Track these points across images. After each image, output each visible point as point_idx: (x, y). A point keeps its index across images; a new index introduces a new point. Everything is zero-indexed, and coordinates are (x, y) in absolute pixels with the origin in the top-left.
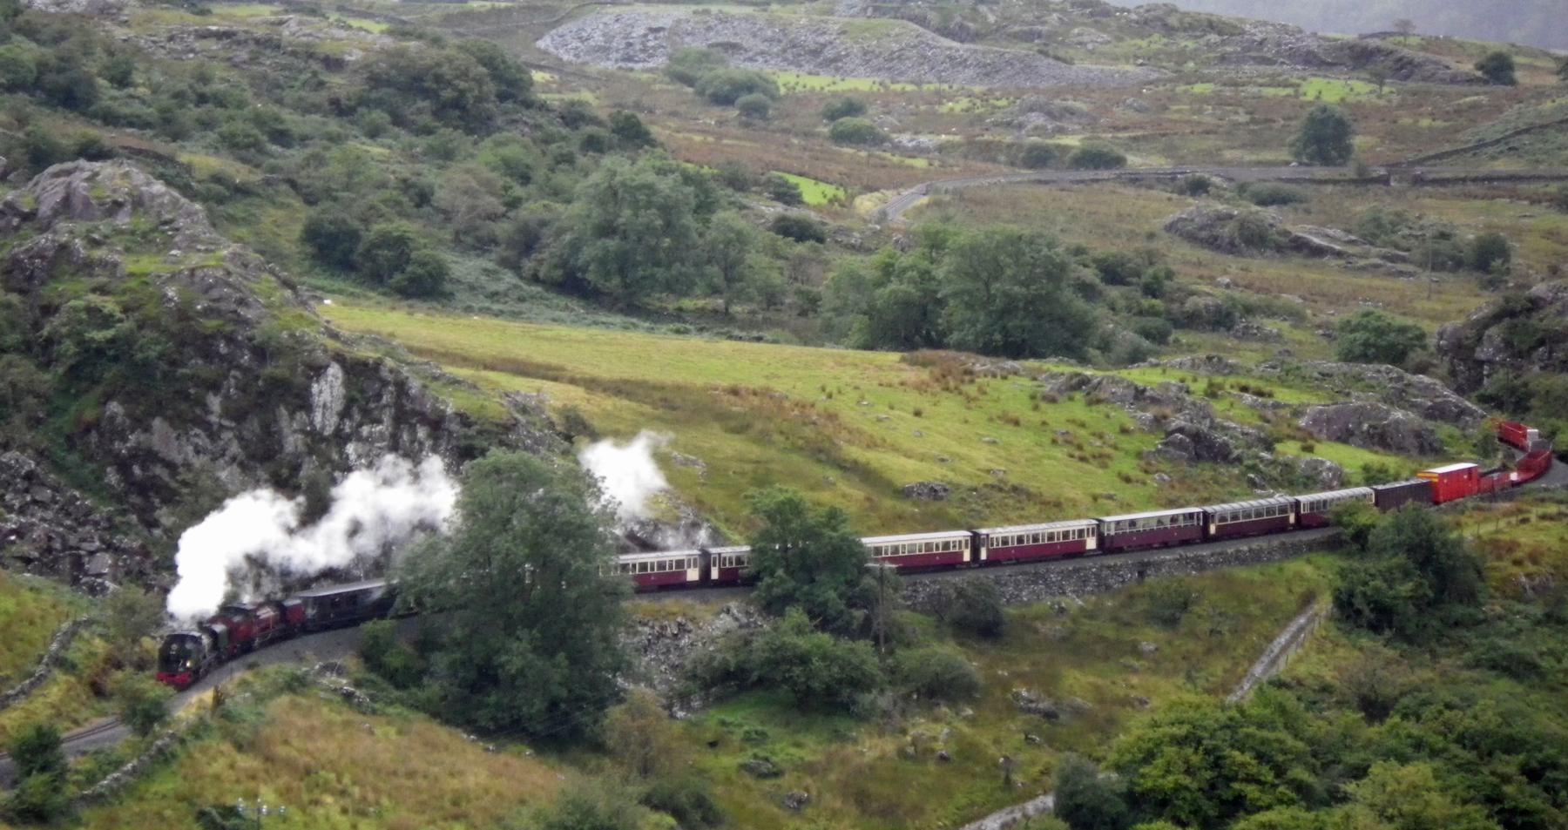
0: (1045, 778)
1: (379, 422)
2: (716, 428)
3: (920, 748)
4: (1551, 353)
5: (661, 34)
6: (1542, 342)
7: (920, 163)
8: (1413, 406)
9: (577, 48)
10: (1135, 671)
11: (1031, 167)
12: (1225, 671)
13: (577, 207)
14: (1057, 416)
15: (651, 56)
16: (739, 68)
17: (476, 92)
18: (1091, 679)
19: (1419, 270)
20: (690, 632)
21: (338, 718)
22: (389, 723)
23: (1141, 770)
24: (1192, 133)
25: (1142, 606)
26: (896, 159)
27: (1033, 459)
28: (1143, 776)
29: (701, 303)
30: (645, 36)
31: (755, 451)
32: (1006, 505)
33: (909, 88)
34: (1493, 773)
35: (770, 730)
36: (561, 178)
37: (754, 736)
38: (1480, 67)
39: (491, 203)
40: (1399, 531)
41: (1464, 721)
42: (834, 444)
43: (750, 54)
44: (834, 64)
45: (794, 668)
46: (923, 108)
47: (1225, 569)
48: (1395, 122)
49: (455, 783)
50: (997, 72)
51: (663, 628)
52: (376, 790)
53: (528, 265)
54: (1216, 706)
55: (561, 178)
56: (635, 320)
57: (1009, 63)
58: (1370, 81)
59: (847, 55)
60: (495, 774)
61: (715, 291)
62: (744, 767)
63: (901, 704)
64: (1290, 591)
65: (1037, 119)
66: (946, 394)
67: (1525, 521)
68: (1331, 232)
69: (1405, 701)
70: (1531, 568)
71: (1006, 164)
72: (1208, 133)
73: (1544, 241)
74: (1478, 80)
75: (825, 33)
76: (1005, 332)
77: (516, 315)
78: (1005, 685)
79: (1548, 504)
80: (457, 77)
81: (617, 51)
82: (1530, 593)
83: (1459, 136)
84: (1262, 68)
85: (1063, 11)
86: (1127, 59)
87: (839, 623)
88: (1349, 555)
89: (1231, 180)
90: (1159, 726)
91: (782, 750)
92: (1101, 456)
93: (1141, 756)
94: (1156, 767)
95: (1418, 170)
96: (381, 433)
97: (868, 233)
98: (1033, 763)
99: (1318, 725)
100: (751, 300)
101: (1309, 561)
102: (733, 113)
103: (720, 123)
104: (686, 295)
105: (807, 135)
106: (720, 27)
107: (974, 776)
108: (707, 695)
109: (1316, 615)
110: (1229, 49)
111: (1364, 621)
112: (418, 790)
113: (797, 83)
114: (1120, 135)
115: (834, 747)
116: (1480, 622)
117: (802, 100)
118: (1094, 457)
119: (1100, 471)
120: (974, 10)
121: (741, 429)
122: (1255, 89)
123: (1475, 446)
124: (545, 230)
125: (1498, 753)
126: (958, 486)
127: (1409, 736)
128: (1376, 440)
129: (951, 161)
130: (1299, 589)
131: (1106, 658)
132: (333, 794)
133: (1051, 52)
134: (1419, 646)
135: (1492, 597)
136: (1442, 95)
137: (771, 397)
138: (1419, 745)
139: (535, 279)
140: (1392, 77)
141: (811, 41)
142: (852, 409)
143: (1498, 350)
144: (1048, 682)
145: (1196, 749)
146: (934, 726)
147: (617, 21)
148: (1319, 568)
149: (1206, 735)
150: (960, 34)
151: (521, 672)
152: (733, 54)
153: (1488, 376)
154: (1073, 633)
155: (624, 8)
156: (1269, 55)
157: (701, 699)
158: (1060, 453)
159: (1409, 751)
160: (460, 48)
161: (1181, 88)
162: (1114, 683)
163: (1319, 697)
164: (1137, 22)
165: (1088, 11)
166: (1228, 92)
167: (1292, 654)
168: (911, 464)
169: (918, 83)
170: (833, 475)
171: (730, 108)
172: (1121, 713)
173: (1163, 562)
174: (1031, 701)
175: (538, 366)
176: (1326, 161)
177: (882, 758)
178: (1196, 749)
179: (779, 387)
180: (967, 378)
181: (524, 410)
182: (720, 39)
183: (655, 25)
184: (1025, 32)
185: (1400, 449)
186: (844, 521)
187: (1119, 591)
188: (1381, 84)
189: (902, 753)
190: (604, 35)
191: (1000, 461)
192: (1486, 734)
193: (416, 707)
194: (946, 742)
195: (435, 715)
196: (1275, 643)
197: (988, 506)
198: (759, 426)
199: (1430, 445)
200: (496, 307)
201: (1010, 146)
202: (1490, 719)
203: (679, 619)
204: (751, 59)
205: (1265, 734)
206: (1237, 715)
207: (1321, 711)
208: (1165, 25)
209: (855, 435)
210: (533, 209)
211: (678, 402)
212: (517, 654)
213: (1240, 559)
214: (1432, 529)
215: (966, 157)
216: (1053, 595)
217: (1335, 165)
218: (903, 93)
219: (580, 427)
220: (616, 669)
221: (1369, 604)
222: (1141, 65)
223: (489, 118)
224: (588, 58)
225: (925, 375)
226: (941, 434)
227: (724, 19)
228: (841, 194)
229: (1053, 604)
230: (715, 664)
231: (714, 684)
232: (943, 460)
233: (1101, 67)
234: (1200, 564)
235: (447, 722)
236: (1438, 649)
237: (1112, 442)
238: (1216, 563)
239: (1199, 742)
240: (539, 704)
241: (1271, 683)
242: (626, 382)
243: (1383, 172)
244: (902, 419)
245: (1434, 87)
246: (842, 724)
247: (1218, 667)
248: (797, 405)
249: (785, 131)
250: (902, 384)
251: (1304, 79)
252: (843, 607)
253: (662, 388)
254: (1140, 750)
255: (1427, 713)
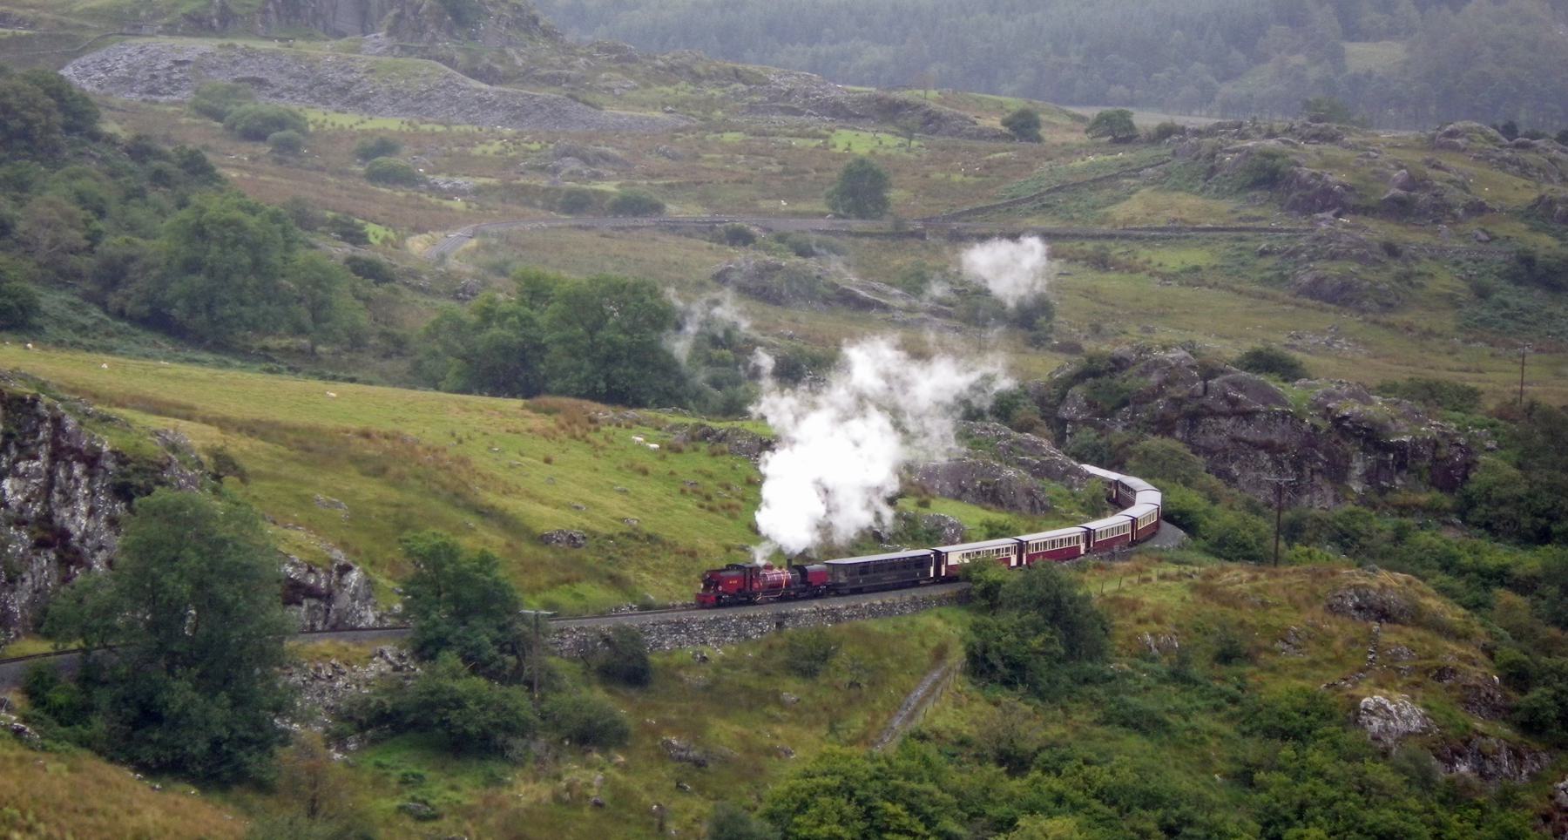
0: (697, 826)
1: (36, 458)
2: (353, 471)
3: (576, 793)
4: (1134, 412)
5: (186, 67)
6: (1125, 403)
7: (458, 204)
8: (1022, 464)
9: (100, 78)
10: (778, 721)
11: (569, 212)
12: (866, 723)
13: (162, 243)
14: (678, 463)
15: (176, 89)
16: (265, 104)
17: (44, 122)
18: (737, 728)
19: (964, 326)
20: (344, 674)
21: (12, 754)
22: (58, 760)
23: (796, 819)
24: (726, 182)
25: (781, 657)
26: (434, 200)
27: (664, 509)
28: (798, 825)
29: (285, 343)
30: (170, 68)
31: (394, 495)
32: (642, 553)
33: (439, 129)
34: (1133, 829)
35: (430, 775)
36: (138, 213)
37: (411, 779)
38: (1005, 123)
39: (76, 236)
40: (1031, 586)
41: (1101, 776)
42: (469, 489)
43: (277, 90)
44: (362, 102)
45: (451, 712)
46: (456, 149)
47: (860, 622)
48: (927, 176)
49: (134, 822)
50: (527, 115)
51: (318, 669)
52: (59, 826)
53: (114, 300)
54: (865, 758)
55: (138, 213)
56: (225, 358)
57: (538, 107)
58: (897, 135)
59: (375, 94)
60: (168, 813)
61: (300, 330)
62: (401, 809)
63: (553, 750)
64: (923, 644)
65: (573, 164)
66: (574, 442)
67: (1146, 580)
68: (875, 285)
69: (1045, 755)
70: (1155, 627)
71: (543, 208)
72: (743, 182)
73: (1083, 299)
74: (1003, 137)
75: (352, 71)
76: (608, 379)
77: (109, 350)
78: (655, 733)
79: (1165, 563)
80: (24, 108)
81: (142, 83)
82: (1155, 651)
83: (992, 191)
84: (789, 118)
85: (590, 56)
86: (654, 105)
87: (492, 667)
88: (981, 610)
89: (769, 230)
90: (813, 777)
91: (439, 793)
92: (730, 506)
93: (795, 806)
94: (810, 818)
95: (955, 225)
96: (37, 468)
97: (437, 276)
98: (686, 811)
99: (957, 777)
100: (337, 341)
101: (940, 616)
102: (264, 149)
103: (254, 159)
104: (267, 333)
105: (342, 173)
106: (246, 62)
107: (628, 821)
108: (363, 738)
109: (950, 669)
110: (756, 98)
111: (998, 677)
112: (99, 828)
113: (325, 121)
114: (656, 182)
115: (490, 791)
116: (1110, 679)
117: (336, 137)
118: (723, 508)
119: (730, 522)
120: (502, 52)
121: (380, 471)
122: (785, 140)
123: (1083, 504)
124: (131, 265)
125: (1136, 809)
126: (594, 534)
127: (1050, 790)
128: (989, 496)
129: (490, 204)
130: (932, 643)
131: (750, 708)
132: (20, 830)
133: (581, 98)
134: (1051, 702)
135: (1119, 655)
136: (972, 150)
137: (403, 441)
138: (1059, 799)
139: (121, 314)
140: (919, 131)
141: (338, 77)
142: (484, 455)
143: (1081, 410)
144: (696, 731)
145: (849, 800)
146: (587, 772)
147: (141, 52)
148: (949, 623)
149: (859, 786)
150: (489, 76)
151: (184, 711)
152: (259, 89)
153: (1071, 435)
154: (716, 682)
155: (147, 40)
156: (796, 106)
157: (357, 741)
158: (690, 504)
159: (1051, 805)
160: (26, 78)
161: (710, 137)
162: (758, 732)
163: (958, 749)
164: (663, 69)
165: (614, 56)
166: (758, 143)
167: (930, 707)
168: (546, 511)
169: (448, 125)
170: (472, 521)
171: (261, 144)
172: (770, 763)
173: (801, 613)
174: (682, 750)
175: (168, 404)
176: (862, 215)
177: (538, 802)
178: (849, 800)
179: (410, 431)
180: (592, 426)
181: (174, 448)
182: (246, 74)
183: (181, 58)
184: (553, 76)
185: (1013, 506)
186: (496, 565)
187: (758, 642)
188: (911, 138)
189: (557, 798)
190: (128, 66)
191: (634, 510)
192: (1124, 790)
193: (84, 743)
194: (600, 789)
195: (100, 753)
196: (912, 696)
197: (625, 555)
198: (394, 469)
199: (1041, 503)
200: (86, 341)
201: (546, 190)
202: (1128, 777)
203: (333, 661)
204: (277, 95)
205: (914, 785)
206: (886, 766)
207: (961, 763)
208: (692, 72)
209: (488, 480)
210: (114, 244)
211: (312, 444)
212: (181, 692)
213: (874, 613)
214: (1061, 585)
215: (503, 201)
216: (694, 644)
217: (873, 218)
218: (433, 134)
219: (230, 467)
220: (278, 709)
221: (1003, 659)
222: (671, 112)
223: (56, 150)
224: (112, 89)
225: (549, 422)
226: (573, 481)
227: (250, 54)
228: (391, 235)
229: (695, 653)
230: (372, 705)
231: (369, 726)
232: (577, 508)
233: (630, 113)
234: (836, 617)
235: (111, 760)
236: (1069, 705)
237: (739, 494)
238: (850, 617)
239: (851, 793)
240: (202, 746)
241: (912, 735)
242: (258, 422)
243: (919, 226)
244: (534, 465)
245: (963, 143)
246: (495, 767)
247: (858, 721)
248: (428, 449)
249: (320, 169)
250: (530, 431)
251: (833, 131)
252: (495, 653)
253: (295, 429)
254: (794, 800)
255: (1067, 768)
